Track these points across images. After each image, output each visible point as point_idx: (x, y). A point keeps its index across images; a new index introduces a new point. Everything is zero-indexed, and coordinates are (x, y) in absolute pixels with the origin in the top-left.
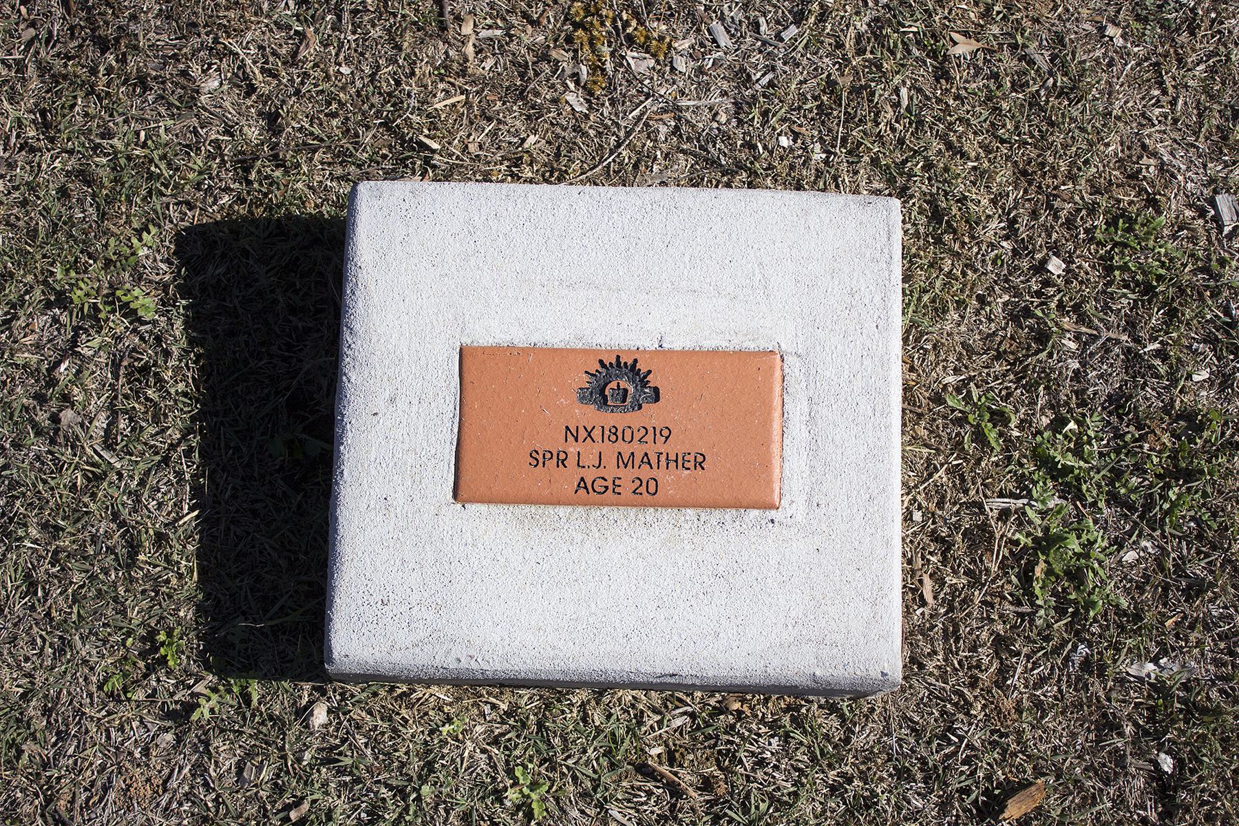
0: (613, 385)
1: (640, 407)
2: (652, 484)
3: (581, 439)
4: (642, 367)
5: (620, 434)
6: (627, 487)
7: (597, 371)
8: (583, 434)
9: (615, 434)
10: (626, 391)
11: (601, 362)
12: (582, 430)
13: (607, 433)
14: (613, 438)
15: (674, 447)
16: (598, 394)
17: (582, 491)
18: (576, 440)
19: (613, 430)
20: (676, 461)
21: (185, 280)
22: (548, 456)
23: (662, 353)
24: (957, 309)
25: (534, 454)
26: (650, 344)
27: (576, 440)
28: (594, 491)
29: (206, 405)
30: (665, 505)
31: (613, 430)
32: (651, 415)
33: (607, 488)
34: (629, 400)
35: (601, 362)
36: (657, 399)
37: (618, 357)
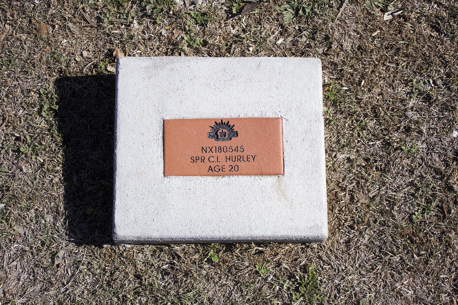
0: (220, 131)
1: (231, 139)
2: (236, 167)
3: (208, 152)
4: (231, 124)
5: (222, 149)
6: (227, 168)
7: (214, 126)
8: (208, 150)
9: (220, 149)
10: (225, 133)
11: (216, 122)
12: (208, 148)
13: (217, 149)
14: (220, 151)
15: (245, 154)
16: (215, 135)
17: (210, 171)
18: (206, 152)
19: (220, 148)
20: (230, 159)
21: (60, 133)
22: (198, 158)
23: (238, 119)
24: (431, 238)
25: (192, 158)
26: (234, 116)
27: (206, 152)
28: (215, 171)
29: (65, 165)
30: (242, 175)
31: (220, 148)
32: (234, 143)
33: (220, 169)
34: (227, 135)
35: (216, 122)
36: (237, 136)
37: (222, 121)
